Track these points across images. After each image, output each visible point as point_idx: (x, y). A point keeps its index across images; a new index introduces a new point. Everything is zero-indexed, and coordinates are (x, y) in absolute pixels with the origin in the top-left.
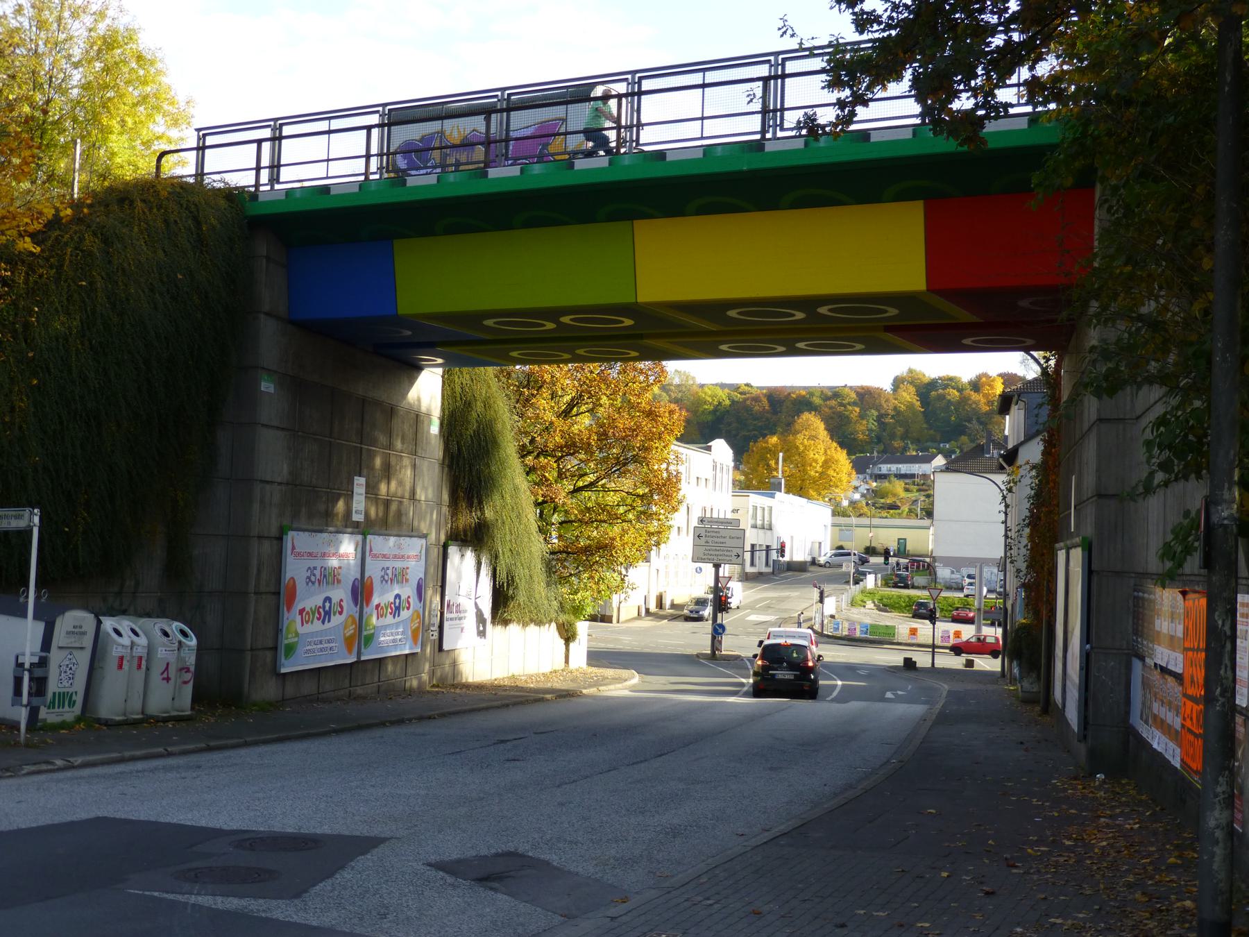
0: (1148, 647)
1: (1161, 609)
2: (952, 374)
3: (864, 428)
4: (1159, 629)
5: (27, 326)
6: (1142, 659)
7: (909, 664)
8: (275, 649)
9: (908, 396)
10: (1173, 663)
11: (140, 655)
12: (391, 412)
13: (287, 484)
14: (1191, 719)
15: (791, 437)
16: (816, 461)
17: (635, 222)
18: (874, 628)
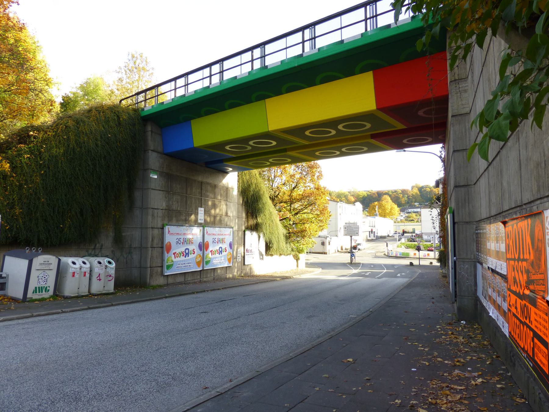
0: (484, 258)
1: (490, 237)
2: (427, 184)
3: (404, 200)
4: (489, 248)
5: (40, 153)
6: (481, 264)
7: (411, 264)
8: (162, 267)
9: (416, 191)
10: (499, 267)
11: (85, 271)
12: (215, 187)
13: (166, 210)
14: (516, 308)
15: (381, 202)
16: (388, 208)
17: (266, 100)
18: (403, 254)
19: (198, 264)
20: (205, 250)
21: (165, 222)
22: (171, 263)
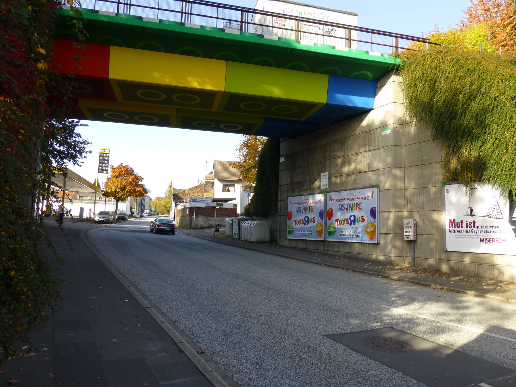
13: (290, 184)
19: (319, 233)
20: (327, 219)
21: (289, 195)
22: (292, 229)
